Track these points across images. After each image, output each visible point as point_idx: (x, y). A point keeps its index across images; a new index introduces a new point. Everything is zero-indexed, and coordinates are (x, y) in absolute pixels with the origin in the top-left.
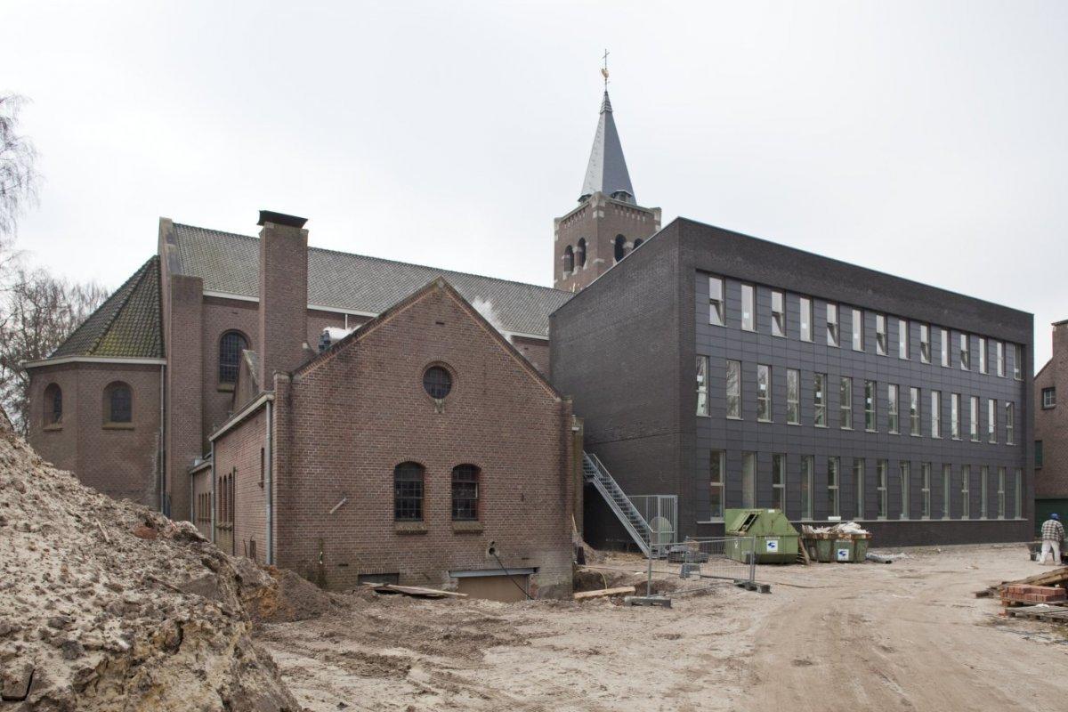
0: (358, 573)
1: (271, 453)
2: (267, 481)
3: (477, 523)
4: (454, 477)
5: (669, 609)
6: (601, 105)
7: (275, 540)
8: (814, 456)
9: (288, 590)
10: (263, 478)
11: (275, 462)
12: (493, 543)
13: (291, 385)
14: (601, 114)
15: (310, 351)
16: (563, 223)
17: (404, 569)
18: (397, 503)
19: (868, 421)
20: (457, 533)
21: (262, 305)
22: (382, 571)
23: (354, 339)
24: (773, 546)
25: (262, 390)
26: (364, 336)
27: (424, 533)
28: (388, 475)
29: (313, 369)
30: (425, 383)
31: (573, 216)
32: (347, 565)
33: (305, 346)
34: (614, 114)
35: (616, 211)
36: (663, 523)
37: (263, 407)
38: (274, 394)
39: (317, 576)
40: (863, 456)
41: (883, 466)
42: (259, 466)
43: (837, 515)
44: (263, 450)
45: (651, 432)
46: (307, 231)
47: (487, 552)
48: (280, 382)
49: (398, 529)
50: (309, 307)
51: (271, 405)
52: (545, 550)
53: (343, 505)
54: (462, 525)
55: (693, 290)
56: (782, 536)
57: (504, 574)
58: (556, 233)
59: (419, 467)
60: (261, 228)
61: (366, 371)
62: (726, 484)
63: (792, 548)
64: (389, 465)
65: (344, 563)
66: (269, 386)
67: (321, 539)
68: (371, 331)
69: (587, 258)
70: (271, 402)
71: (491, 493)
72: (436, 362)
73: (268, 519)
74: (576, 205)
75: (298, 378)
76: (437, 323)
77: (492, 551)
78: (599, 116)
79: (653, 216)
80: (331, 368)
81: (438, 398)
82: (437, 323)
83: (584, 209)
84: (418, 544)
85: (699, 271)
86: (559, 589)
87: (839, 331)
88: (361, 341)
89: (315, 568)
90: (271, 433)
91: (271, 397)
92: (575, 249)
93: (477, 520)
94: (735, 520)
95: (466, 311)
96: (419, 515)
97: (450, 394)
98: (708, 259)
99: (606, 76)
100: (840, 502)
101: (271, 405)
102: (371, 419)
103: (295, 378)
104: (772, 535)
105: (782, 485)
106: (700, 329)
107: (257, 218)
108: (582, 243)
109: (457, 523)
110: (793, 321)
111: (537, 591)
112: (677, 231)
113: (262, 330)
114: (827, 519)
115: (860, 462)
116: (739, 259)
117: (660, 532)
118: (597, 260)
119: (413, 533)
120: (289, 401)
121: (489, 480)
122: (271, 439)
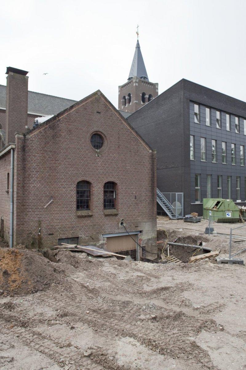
0: (58, 238)
1: (13, 176)
2: (11, 190)
3: (115, 210)
4: (105, 187)
5: (242, 266)
6: (136, 45)
7: (15, 222)
8: (240, 177)
9: (27, 267)
10: (8, 188)
11: (15, 181)
12: (123, 220)
13: (25, 140)
14: (136, 48)
15: (28, 129)
16: (122, 88)
17: (82, 235)
18: (78, 202)
19: (232, 161)
20: (106, 215)
21: (7, 111)
22: (70, 236)
23: (57, 118)
24: (229, 215)
25: (7, 145)
26: (62, 117)
27: (91, 216)
28: (74, 187)
29: (36, 132)
30: (91, 142)
31: (124, 86)
32: (53, 234)
33: (26, 127)
34: (141, 48)
35: (142, 83)
36: (178, 203)
37: (9, 152)
38: (15, 145)
39: (37, 241)
40: (240, 176)
41: (238, 179)
42: (6, 182)
43: (239, 200)
44: (8, 174)
45: (170, 167)
46: (28, 77)
47: (120, 225)
48: (19, 138)
49: (78, 215)
50: (28, 113)
51: (14, 151)
52: (146, 222)
53: (51, 203)
54: (108, 211)
55: (188, 108)
56: (233, 211)
57: (127, 234)
58: (119, 91)
59: (88, 183)
60: (7, 75)
61: (63, 134)
62: (201, 188)
63: (237, 216)
64: (74, 182)
65: (51, 233)
66: (11, 140)
67: (40, 221)
68: (66, 114)
69: (131, 100)
70: (13, 149)
71: (122, 196)
72: (96, 131)
73: (11, 211)
74: (126, 81)
75: (28, 136)
76: (97, 112)
77: (122, 223)
78: (135, 49)
79: (155, 86)
80: (46, 133)
81: (97, 149)
82: (97, 112)
83: (130, 82)
84: (87, 222)
85: (191, 101)
86: (151, 240)
87: (239, 127)
88: (60, 119)
89: (37, 237)
90: (13, 165)
91: (14, 146)
92: (127, 97)
93: (115, 209)
94: (209, 203)
95: (110, 107)
96: (88, 207)
97: (103, 148)
98: (194, 97)
99: (138, 34)
100: (240, 195)
101: (14, 151)
102: (65, 159)
103: (27, 136)
104: (229, 210)
105: (220, 188)
106: (191, 124)
107: (6, 71)
108: (129, 95)
109: (105, 210)
110: (224, 123)
111: (142, 242)
112: (182, 84)
113: (7, 120)
114: (236, 201)
115: (229, 178)
116: (205, 97)
117: (177, 208)
118: (135, 101)
119: (85, 216)
120: (24, 149)
121: (121, 188)
122: (13, 168)
